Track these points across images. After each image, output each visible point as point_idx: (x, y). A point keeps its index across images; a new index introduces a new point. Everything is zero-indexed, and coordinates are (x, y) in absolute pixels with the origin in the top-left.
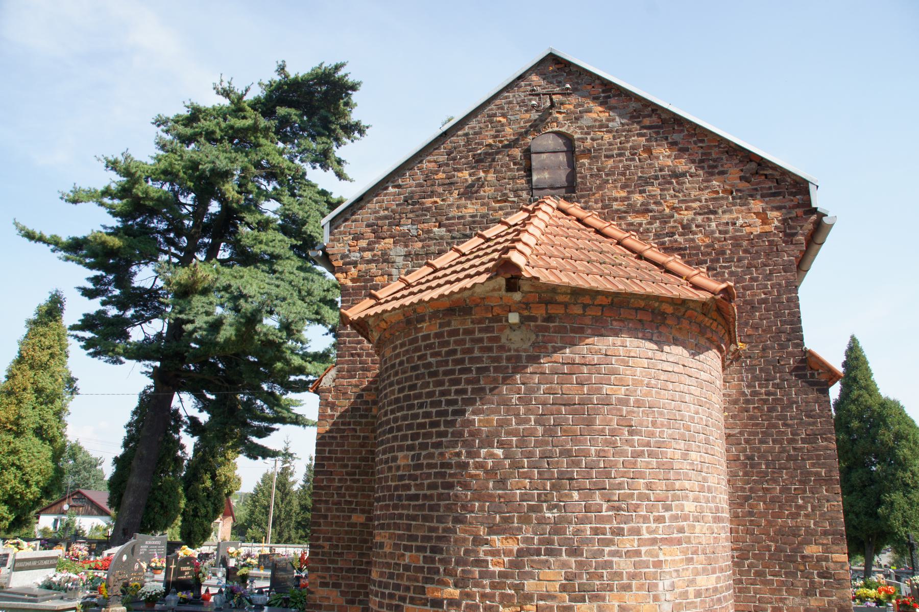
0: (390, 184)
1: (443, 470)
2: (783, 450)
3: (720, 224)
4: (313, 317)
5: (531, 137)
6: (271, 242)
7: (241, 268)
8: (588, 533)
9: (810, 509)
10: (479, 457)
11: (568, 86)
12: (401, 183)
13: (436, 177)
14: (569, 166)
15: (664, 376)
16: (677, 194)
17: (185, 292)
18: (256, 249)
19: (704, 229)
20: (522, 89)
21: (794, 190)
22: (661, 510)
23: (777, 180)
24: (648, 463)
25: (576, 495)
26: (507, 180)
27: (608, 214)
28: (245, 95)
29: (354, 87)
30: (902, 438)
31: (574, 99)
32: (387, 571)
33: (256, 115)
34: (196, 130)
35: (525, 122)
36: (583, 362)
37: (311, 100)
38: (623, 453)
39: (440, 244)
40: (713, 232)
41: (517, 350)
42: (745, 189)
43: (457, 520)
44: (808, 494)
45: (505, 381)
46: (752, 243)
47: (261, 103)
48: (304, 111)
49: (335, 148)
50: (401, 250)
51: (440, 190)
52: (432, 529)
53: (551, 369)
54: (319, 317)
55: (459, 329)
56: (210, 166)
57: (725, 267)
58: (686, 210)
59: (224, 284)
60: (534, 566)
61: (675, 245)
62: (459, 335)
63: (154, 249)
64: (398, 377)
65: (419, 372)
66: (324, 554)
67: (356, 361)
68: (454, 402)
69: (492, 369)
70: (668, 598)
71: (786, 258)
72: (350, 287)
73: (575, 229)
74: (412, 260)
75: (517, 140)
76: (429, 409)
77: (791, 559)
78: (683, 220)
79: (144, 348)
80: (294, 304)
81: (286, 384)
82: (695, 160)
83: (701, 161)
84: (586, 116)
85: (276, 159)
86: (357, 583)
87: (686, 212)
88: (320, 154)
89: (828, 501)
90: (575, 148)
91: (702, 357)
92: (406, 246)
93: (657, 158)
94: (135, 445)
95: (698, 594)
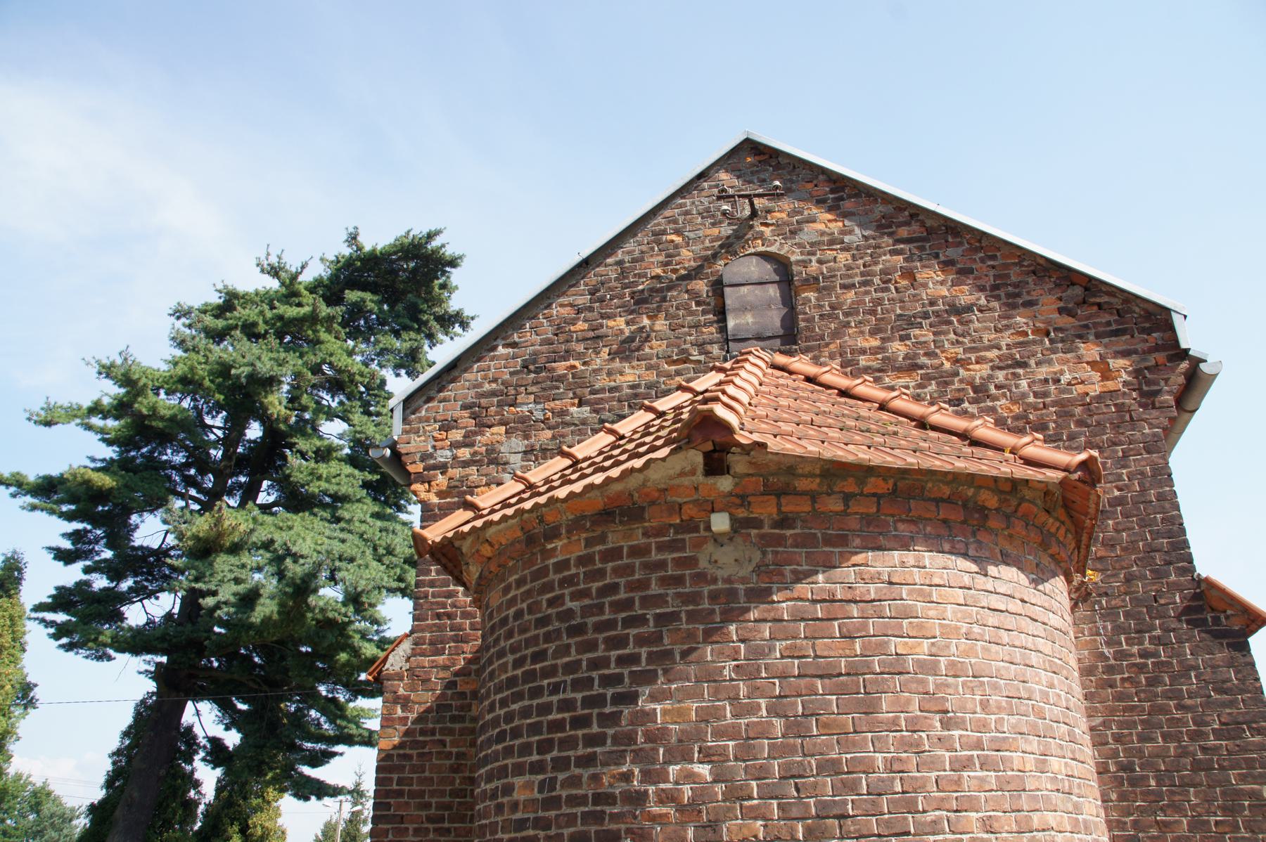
0: (500, 342)
1: (598, 808)
2: (1184, 753)
3: (1034, 382)
4: (395, 585)
5: (722, 262)
6: (334, 477)
7: (289, 515)
11: (777, 183)
13: (572, 328)
14: (784, 304)
15: (993, 619)
16: (961, 339)
17: (204, 550)
18: (314, 488)
19: (1010, 391)
20: (704, 193)
21: (1147, 325)
23: (1118, 310)
24: (982, 779)
26: (686, 329)
28: (301, 273)
29: (453, 263)
31: (786, 204)
33: (315, 299)
34: (231, 322)
36: (849, 597)
37: (394, 282)
38: (934, 764)
40: (1024, 396)
41: (728, 580)
42: (1068, 326)
45: (711, 636)
46: (1089, 410)
47: (324, 286)
48: (383, 297)
49: (426, 348)
50: (518, 444)
55: (622, 547)
56: (247, 370)
58: (977, 363)
59: (264, 539)
62: (621, 558)
63: (163, 490)
64: (512, 641)
65: (550, 628)
68: (618, 679)
69: (683, 616)
71: (1147, 431)
72: (434, 505)
75: (701, 267)
76: (570, 695)
78: (974, 379)
79: (144, 635)
80: (367, 566)
81: (353, 686)
82: (984, 286)
83: (995, 287)
84: (808, 228)
85: (342, 361)
87: (977, 367)
88: (406, 355)
92: (527, 437)
93: (925, 286)
94: (124, 784)
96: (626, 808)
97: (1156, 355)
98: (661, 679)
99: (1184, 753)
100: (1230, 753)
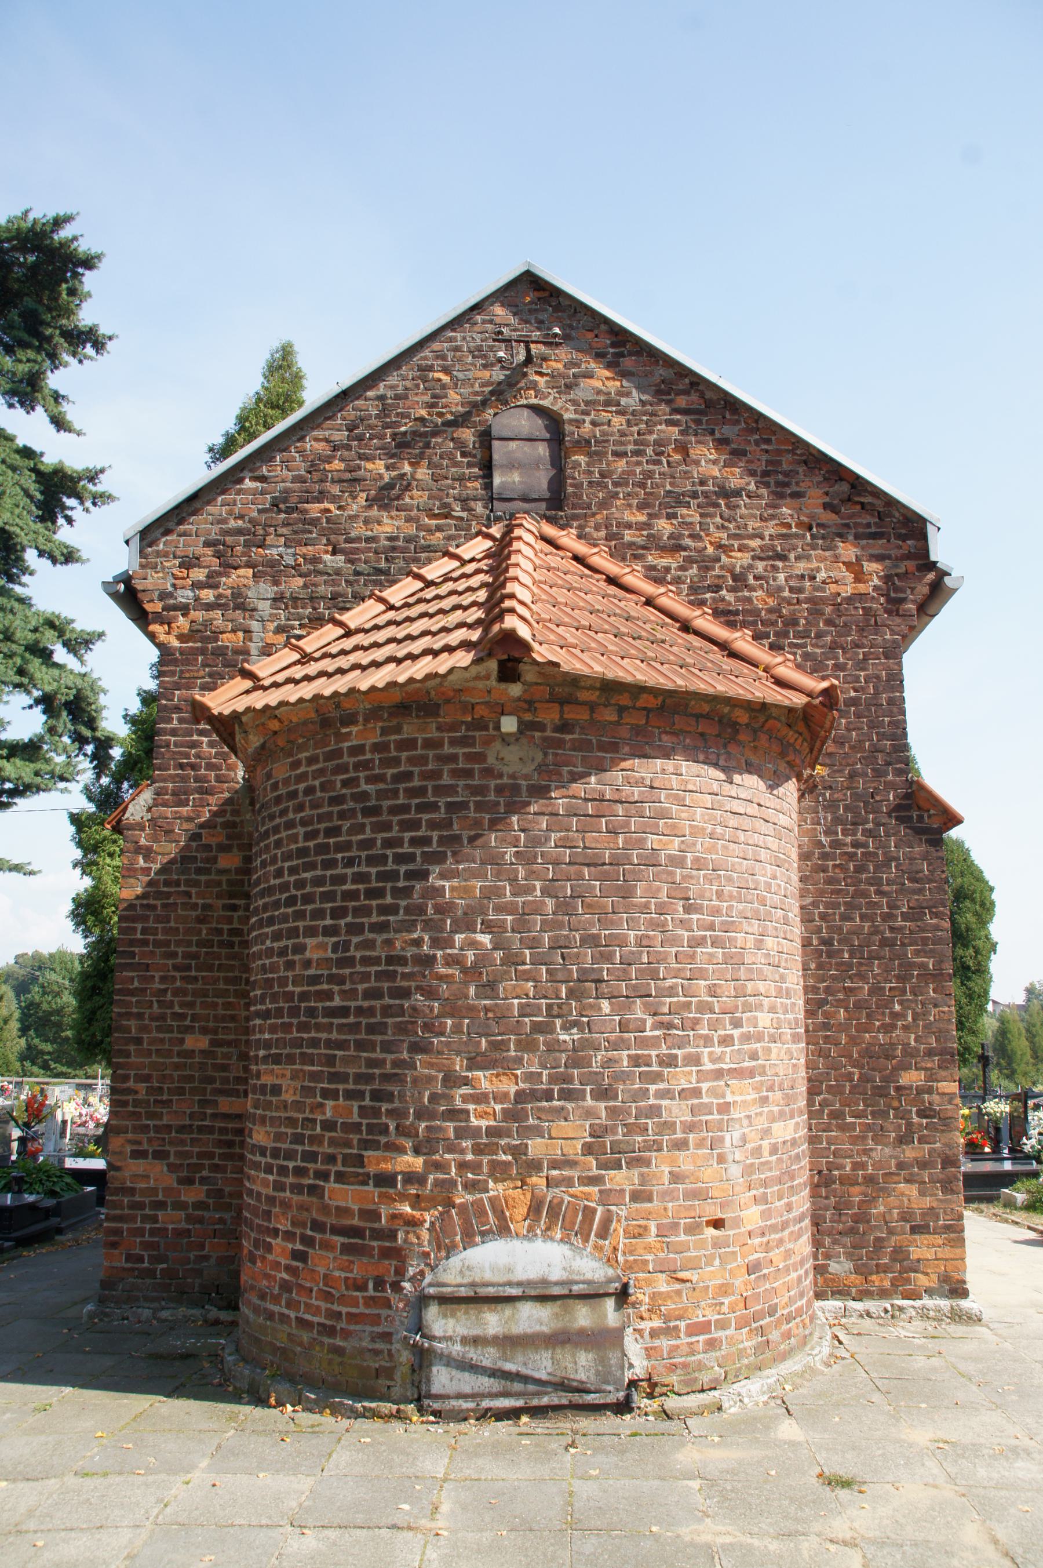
0: (247, 474)
2: (875, 931)
3: (791, 577)
4: (17, 679)
5: (491, 411)
8: (625, 1063)
9: (910, 1019)
11: (557, 330)
12: (266, 473)
13: (327, 467)
14: (553, 465)
15: (733, 822)
16: (726, 524)
20: (477, 328)
21: (903, 531)
22: (728, 1027)
24: (711, 955)
27: (621, 552)
29: (89, 263)
30: (966, 897)
31: (564, 353)
32: (289, 1131)
35: (482, 385)
38: (675, 941)
39: (334, 583)
40: (780, 589)
41: (512, 776)
43: (416, 1048)
44: (909, 996)
50: (267, 590)
51: (336, 490)
52: (372, 1063)
54: (25, 680)
57: (797, 646)
58: (740, 550)
60: (543, 1117)
62: (416, 749)
64: (303, 814)
65: (345, 807)
66: (137, 1103)
67: (188, 776)
68: (410, 858)
69: (471, 805)
70: (737, 1158)
71: (888, 637)
72: (176, 648)
73: (576, 574)
74: (287, 608)
76: (364, 869)
77: (881, 1092)
78: (734, 566)
83: (765, 474)
84: (584, 383)
86: (196, 1150)
87: (739, 555)
89: (935, 1006)
90: (564, 435)
92: (276, 583)
93: (697, 463)
95: (774, 1150)
96: (416, 969)
98: (450, 860)
99: (875, 931)
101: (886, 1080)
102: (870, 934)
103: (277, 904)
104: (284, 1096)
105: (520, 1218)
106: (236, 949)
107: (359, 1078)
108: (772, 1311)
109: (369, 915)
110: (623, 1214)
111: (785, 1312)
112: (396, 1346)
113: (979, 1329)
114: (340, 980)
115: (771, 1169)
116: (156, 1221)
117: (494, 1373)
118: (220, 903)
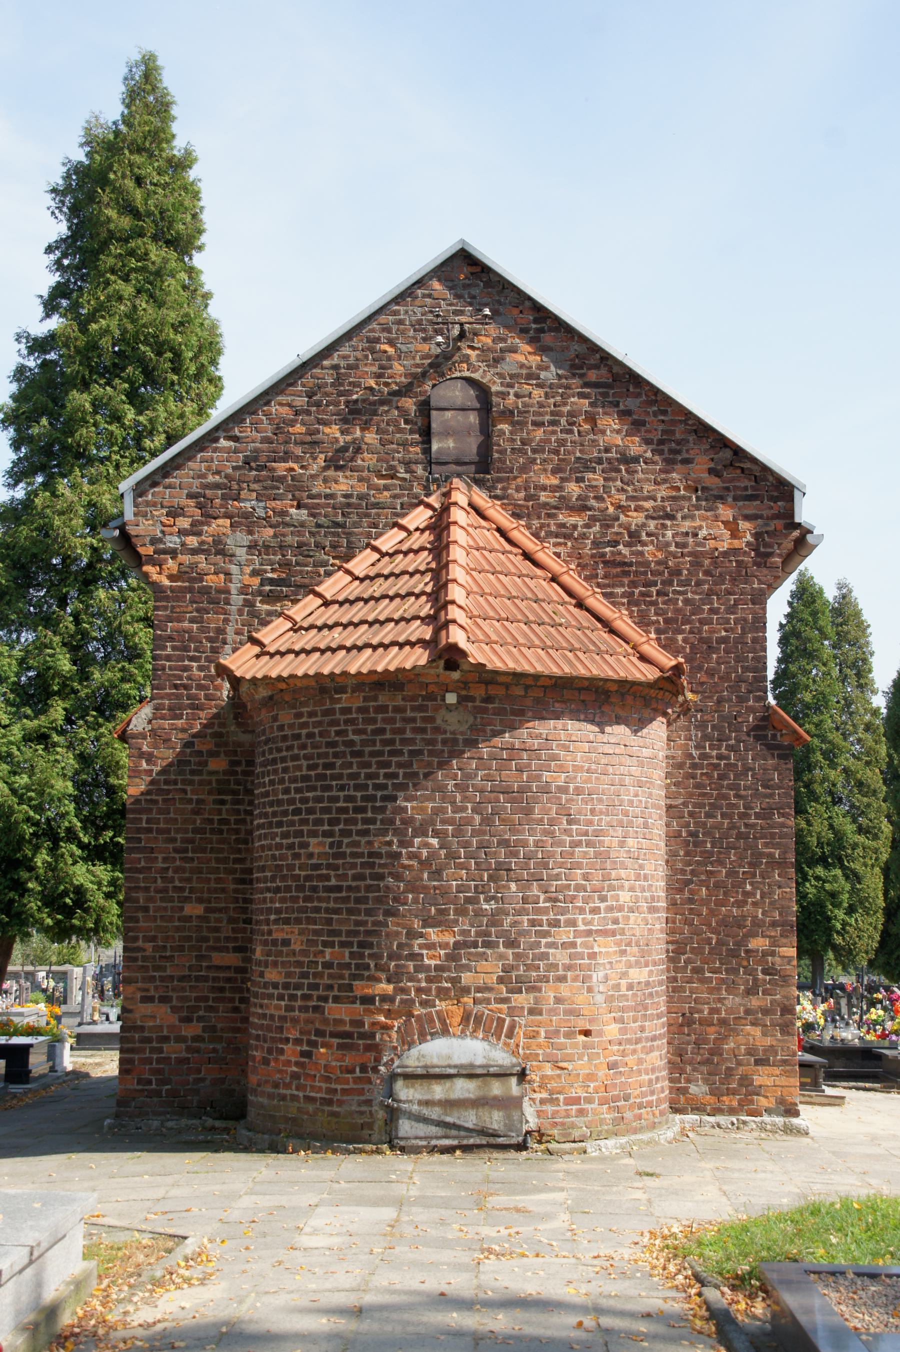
0: (221, 434)
2: (733, 826)
5: (430, 383)
9: (758, 897)
10: (413, 846)
12: (238, 434)
14: (481, 432)
15: (604, 760)
16: (625, 487)
20: (418, 302)
21: (775, 494)
24: (585, 852)
25: (513, 886)
26: (395, 446)
31: (493, 329)
32: (297, 970)
35: (422, 358)
38: (561, 843)
39: (299, 534)
40: (668, 544)
41: (453, 733)
43: (389, 913)
46: (716, 563)
50: (243, 538)
51: (298, 451)
52: (358, 923)
53: (489, 754)
57: (679, 593)
58: (636, 510)
61: (618, 558)
66: (145, 959)
68: (384, 787)
70: (601, 989)
71: (755, 586)
75: (411, 384)
76: (352, 793)
77: (734, 954)
78: (630, 525)
83: (661, 442)
84: (510, 357)
86: (194, 995)
87: (635, 514)
89: (779, 887)
91: (645, 731)
92: (251, 533)
93: (603, 432)
95: (630, 987)
97: (776, 522)
99: (733, 826)
100: (762, 828)
101: (738, 944)
102: (729, 829)
103: (285, 813)
104: (292, 947)
105: (456, 1024)
106: (225, 835)
107: (349, 933)
108: (627, 1098)
109: (356, 824)
110: (523, 1022)
111: (638, 1101)
112: (375, 1108)
113: (805, 1140)
114: (336, 868)
115: (627, 1000)
116: (162, 1052)
117: (440, 1124)
118: (211, 798)
